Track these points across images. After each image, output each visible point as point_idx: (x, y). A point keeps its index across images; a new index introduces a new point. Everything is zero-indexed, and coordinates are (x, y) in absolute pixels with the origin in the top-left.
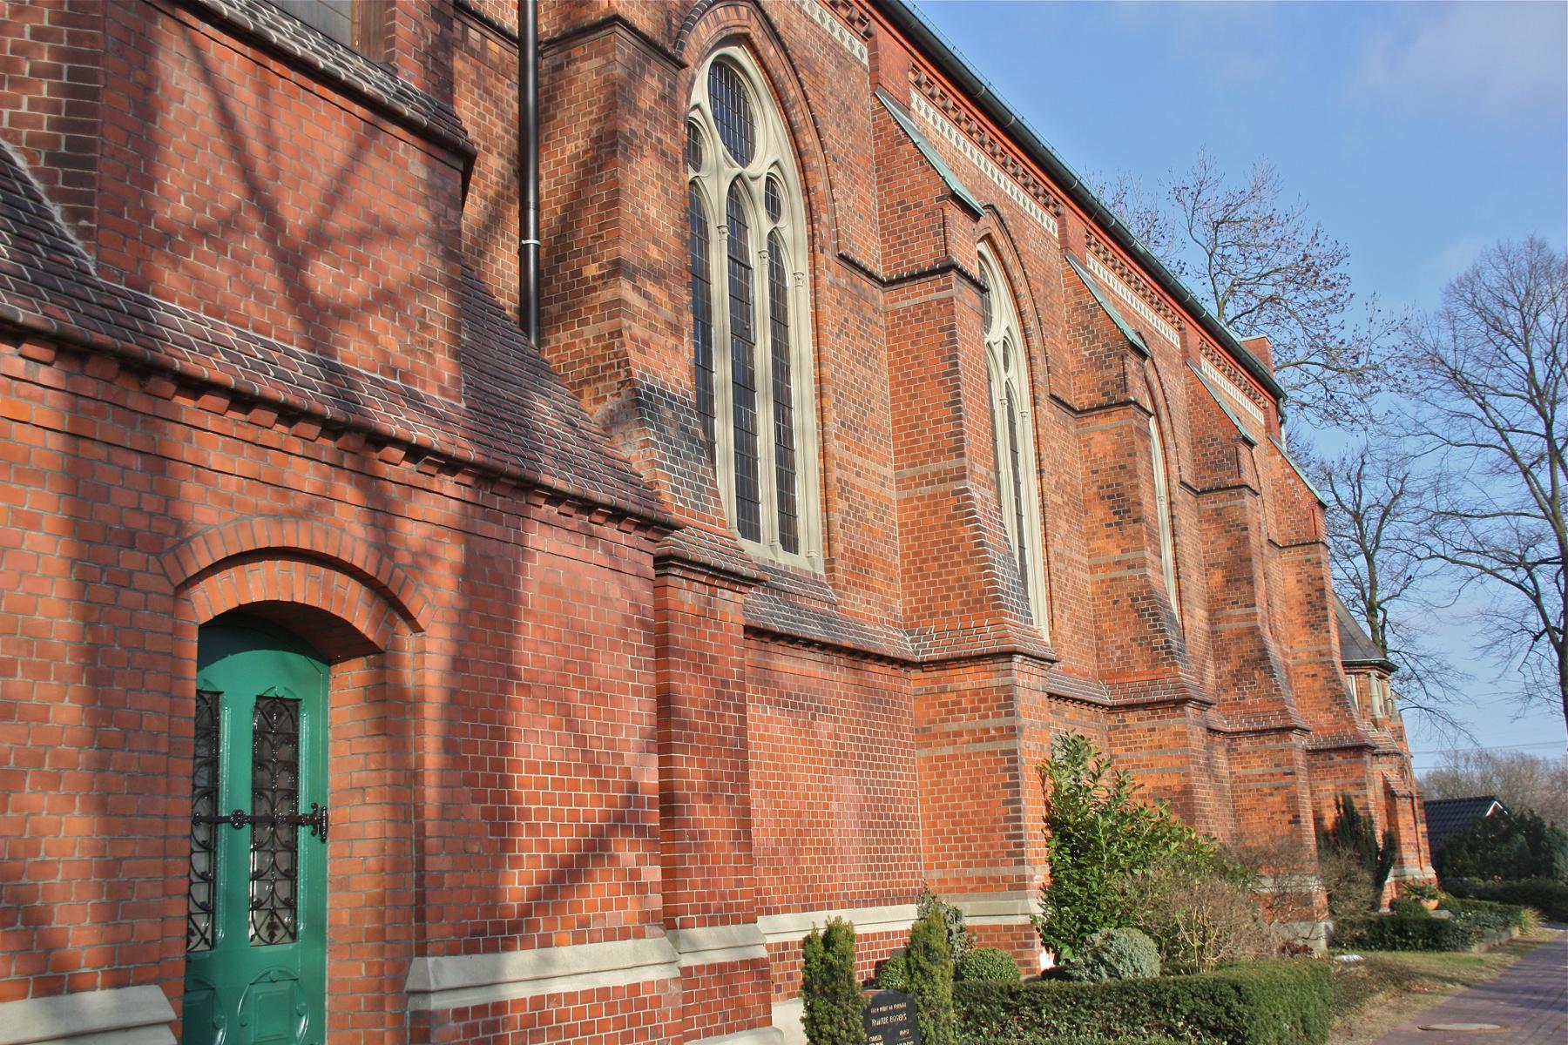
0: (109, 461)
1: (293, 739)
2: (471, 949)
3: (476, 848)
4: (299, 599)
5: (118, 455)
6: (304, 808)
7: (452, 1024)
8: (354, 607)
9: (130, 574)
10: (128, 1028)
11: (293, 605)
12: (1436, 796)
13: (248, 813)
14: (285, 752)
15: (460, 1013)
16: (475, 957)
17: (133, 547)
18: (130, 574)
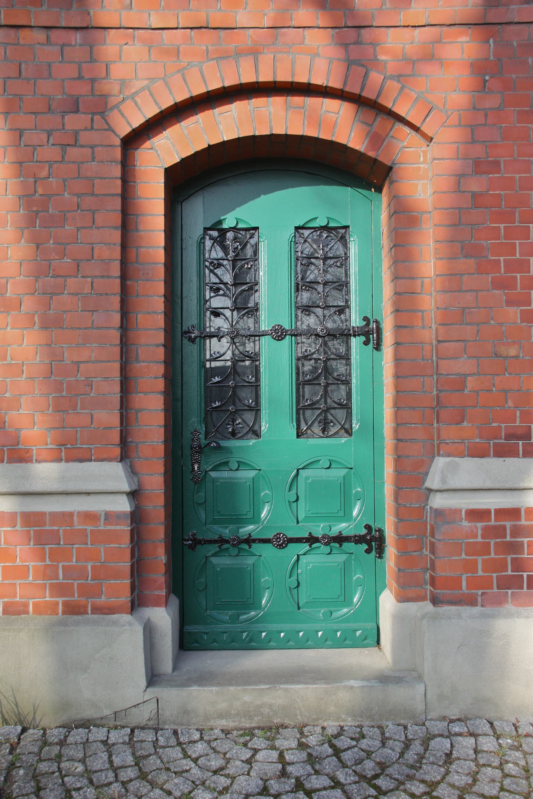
0: (48, 41)
1: (343, 261)
2: (502, 452)
3: (512, 352)
4: (279, 130)
5: (54, 34)
6: (356, 321)
7: (465, 523)
8: (338, 124)
9: (76, 133)
10: (89, 494)
11: (272, 138)
12: (163, 618)
13: (287, 327)
14: (334, 273)
15: (476, 515)
16: (510, 461)
17: (77, 111)
18: (76, 133)
